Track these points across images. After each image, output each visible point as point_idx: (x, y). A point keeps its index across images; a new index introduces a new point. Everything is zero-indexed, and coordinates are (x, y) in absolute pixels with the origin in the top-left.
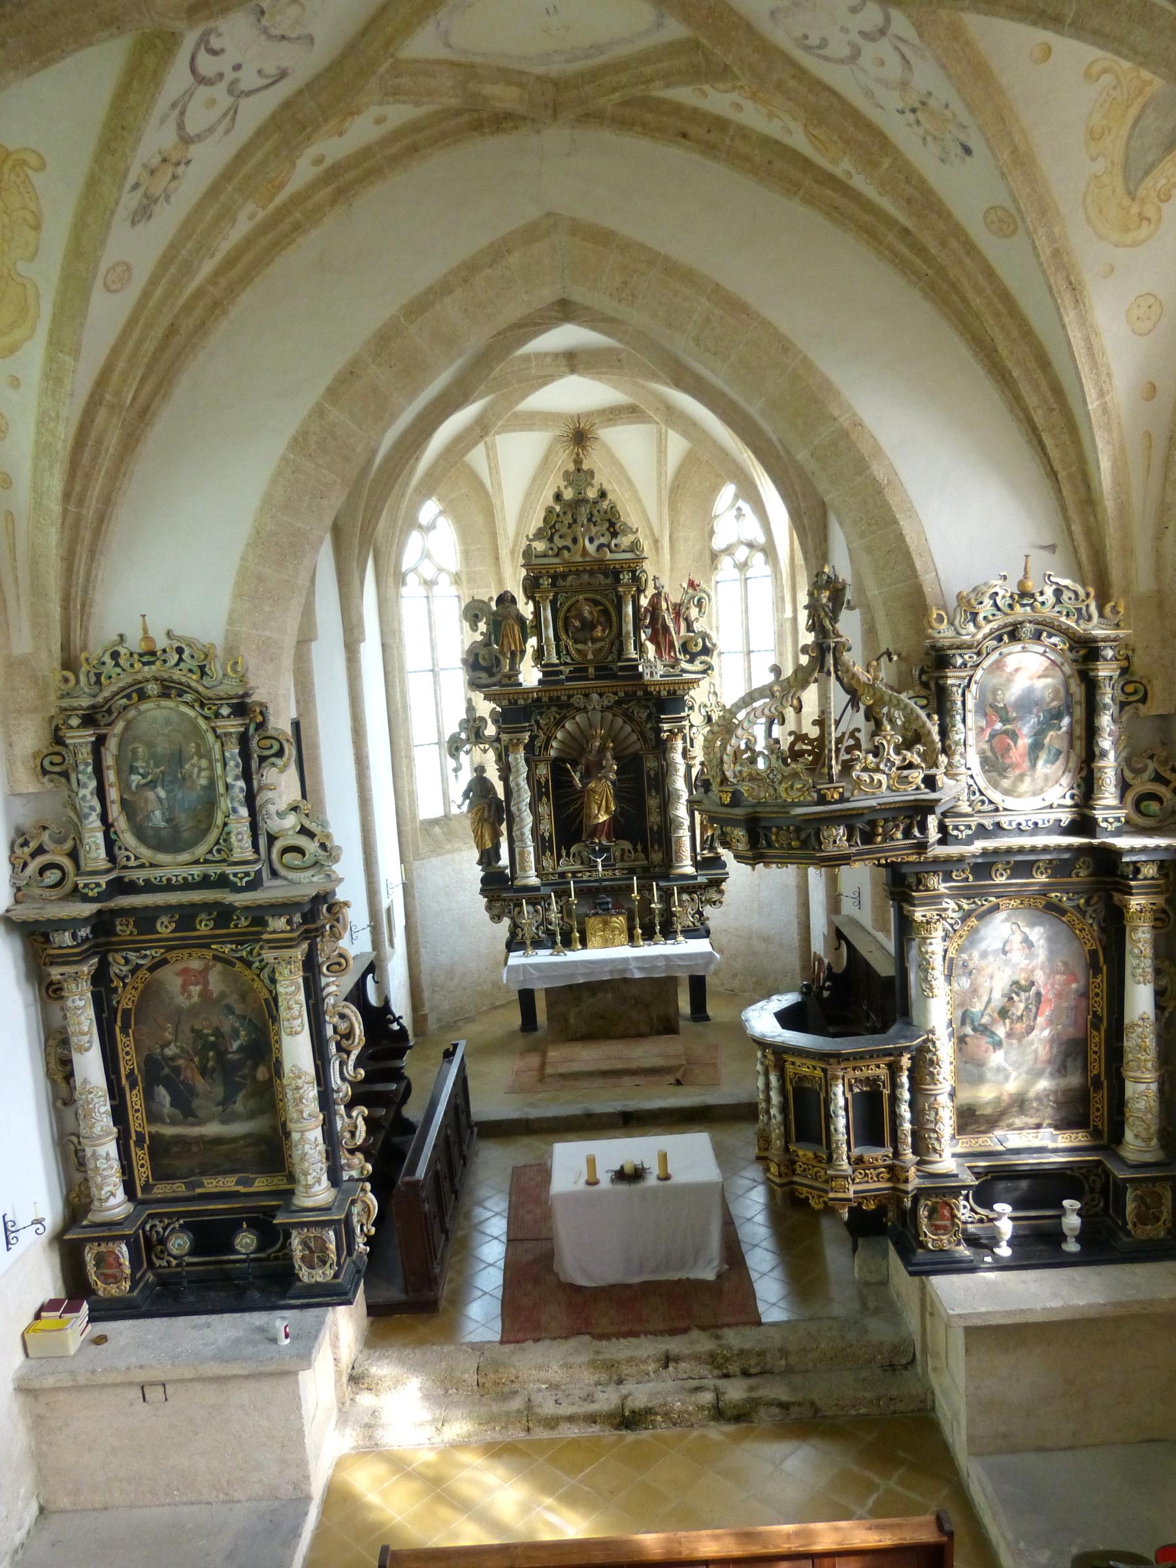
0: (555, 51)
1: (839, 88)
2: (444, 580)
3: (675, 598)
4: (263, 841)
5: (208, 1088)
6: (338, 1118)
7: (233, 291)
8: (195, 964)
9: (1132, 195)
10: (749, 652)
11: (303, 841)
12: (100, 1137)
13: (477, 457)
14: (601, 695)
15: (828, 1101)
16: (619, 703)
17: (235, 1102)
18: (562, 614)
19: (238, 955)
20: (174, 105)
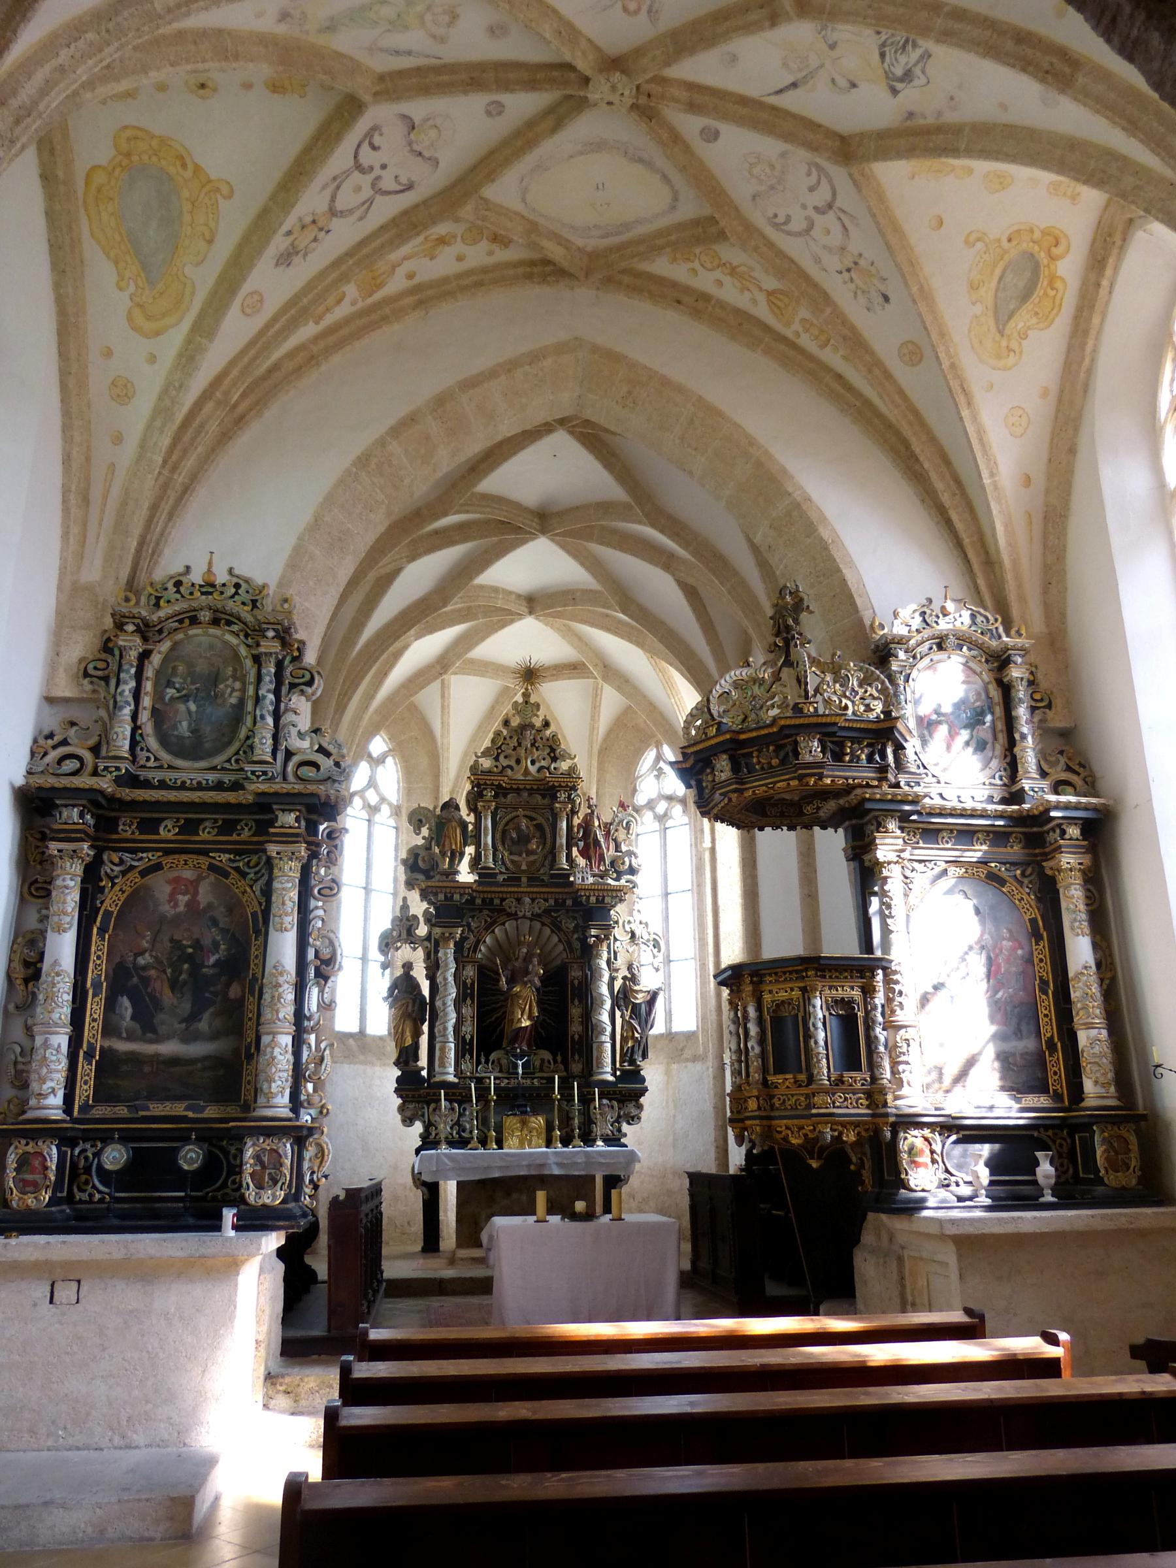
0: (595, 226)
1: (796, 257)
2: (385, 810)
3: (606, 817)
4: (280, 756)
5: (175, 1002)
6: (305, 1048)
7: (328, 351)
8: (188, 874)
9: (1001, 333)
10: (667, 894)
11: (320, 759)
12: (56, 1025)
13: (428, 697)
14: (533, 900)
15: (807, 1016)
16: (547, 912)
17: (200, 1020)
18: (500, 827)
19: (235, 865)
20: (335, 179)
